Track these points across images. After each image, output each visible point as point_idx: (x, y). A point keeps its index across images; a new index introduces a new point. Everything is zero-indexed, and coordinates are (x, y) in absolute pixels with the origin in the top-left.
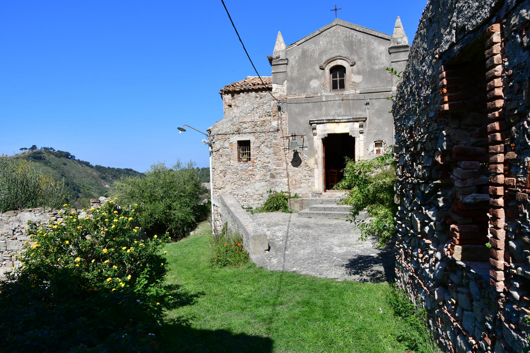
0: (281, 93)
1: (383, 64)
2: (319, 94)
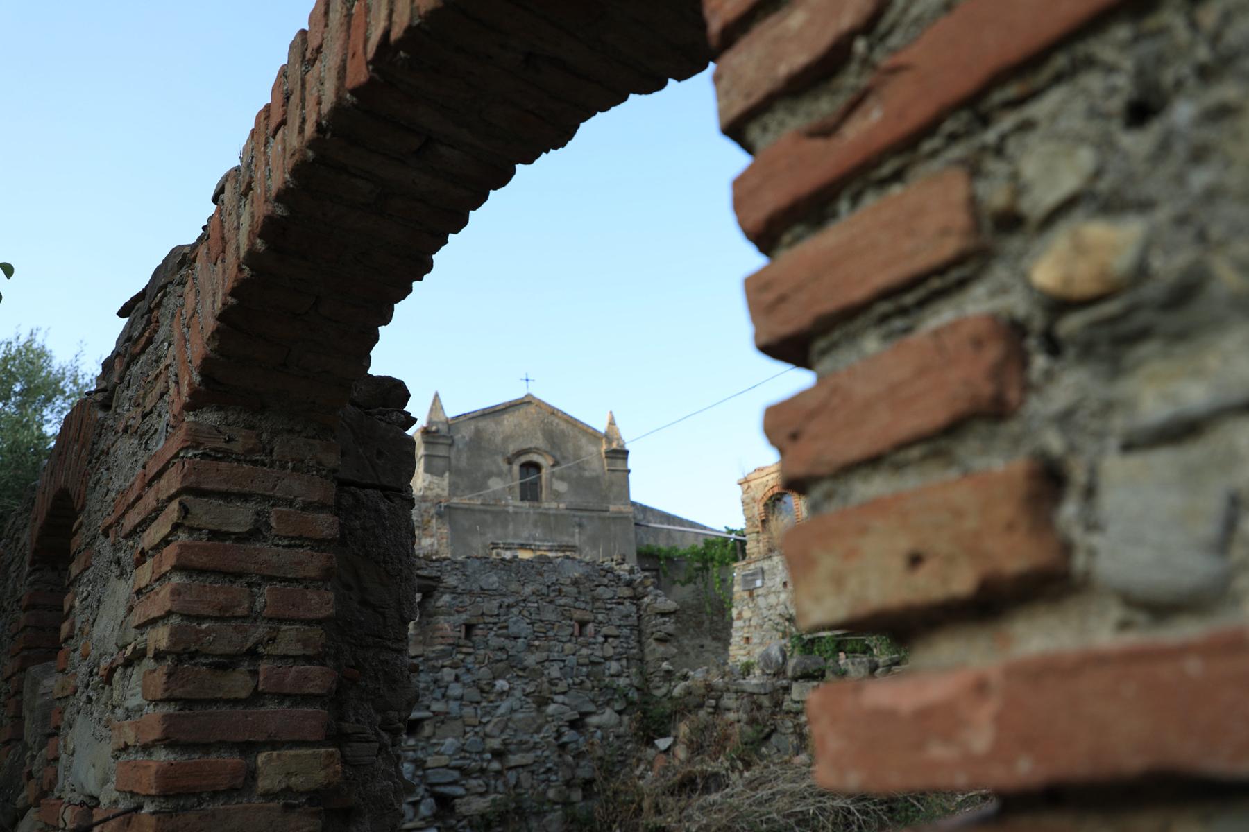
0: (438, 491)
1: (594, 471)
2: (503, 502)
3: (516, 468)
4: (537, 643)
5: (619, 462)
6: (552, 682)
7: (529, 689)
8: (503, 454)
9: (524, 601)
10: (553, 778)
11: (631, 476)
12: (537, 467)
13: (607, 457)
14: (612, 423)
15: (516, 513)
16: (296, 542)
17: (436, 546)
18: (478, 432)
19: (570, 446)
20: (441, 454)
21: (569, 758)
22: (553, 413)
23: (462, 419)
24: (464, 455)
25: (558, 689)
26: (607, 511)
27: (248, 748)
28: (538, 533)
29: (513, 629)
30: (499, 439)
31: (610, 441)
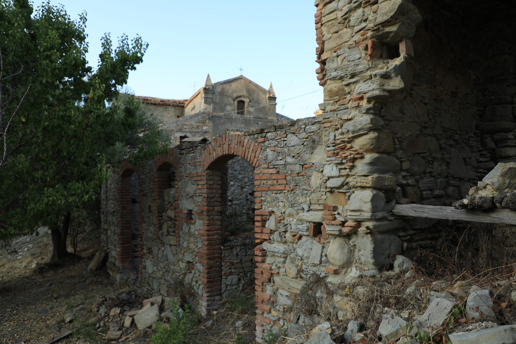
0: (209, 110)
1: (264, 104)
3: (236, 103)
4: (242, 172)
5: (273, 101)
6: (245, 183)
7: (239, 184)
8: (232, 97)
9: (239, 161)
10: (245, 207)
11: (277, 106)
12: (243, 102)
13: (269, 99)
14: (271, 87)
15: (235, 119)
16: (217, 185)
17: (208, 130)
18: (223, 89)
19: (255, 95)
20: (210, 97)
21: (249, 203)
22: (250, 83)
23: (217, 84)
24: (218, 97)
25: (247, 185)
26: (267, 119)
27: (214, 207)
28: (243, 126)
29: (235, 169)
30: (230, 92)
31: (270, 94)
